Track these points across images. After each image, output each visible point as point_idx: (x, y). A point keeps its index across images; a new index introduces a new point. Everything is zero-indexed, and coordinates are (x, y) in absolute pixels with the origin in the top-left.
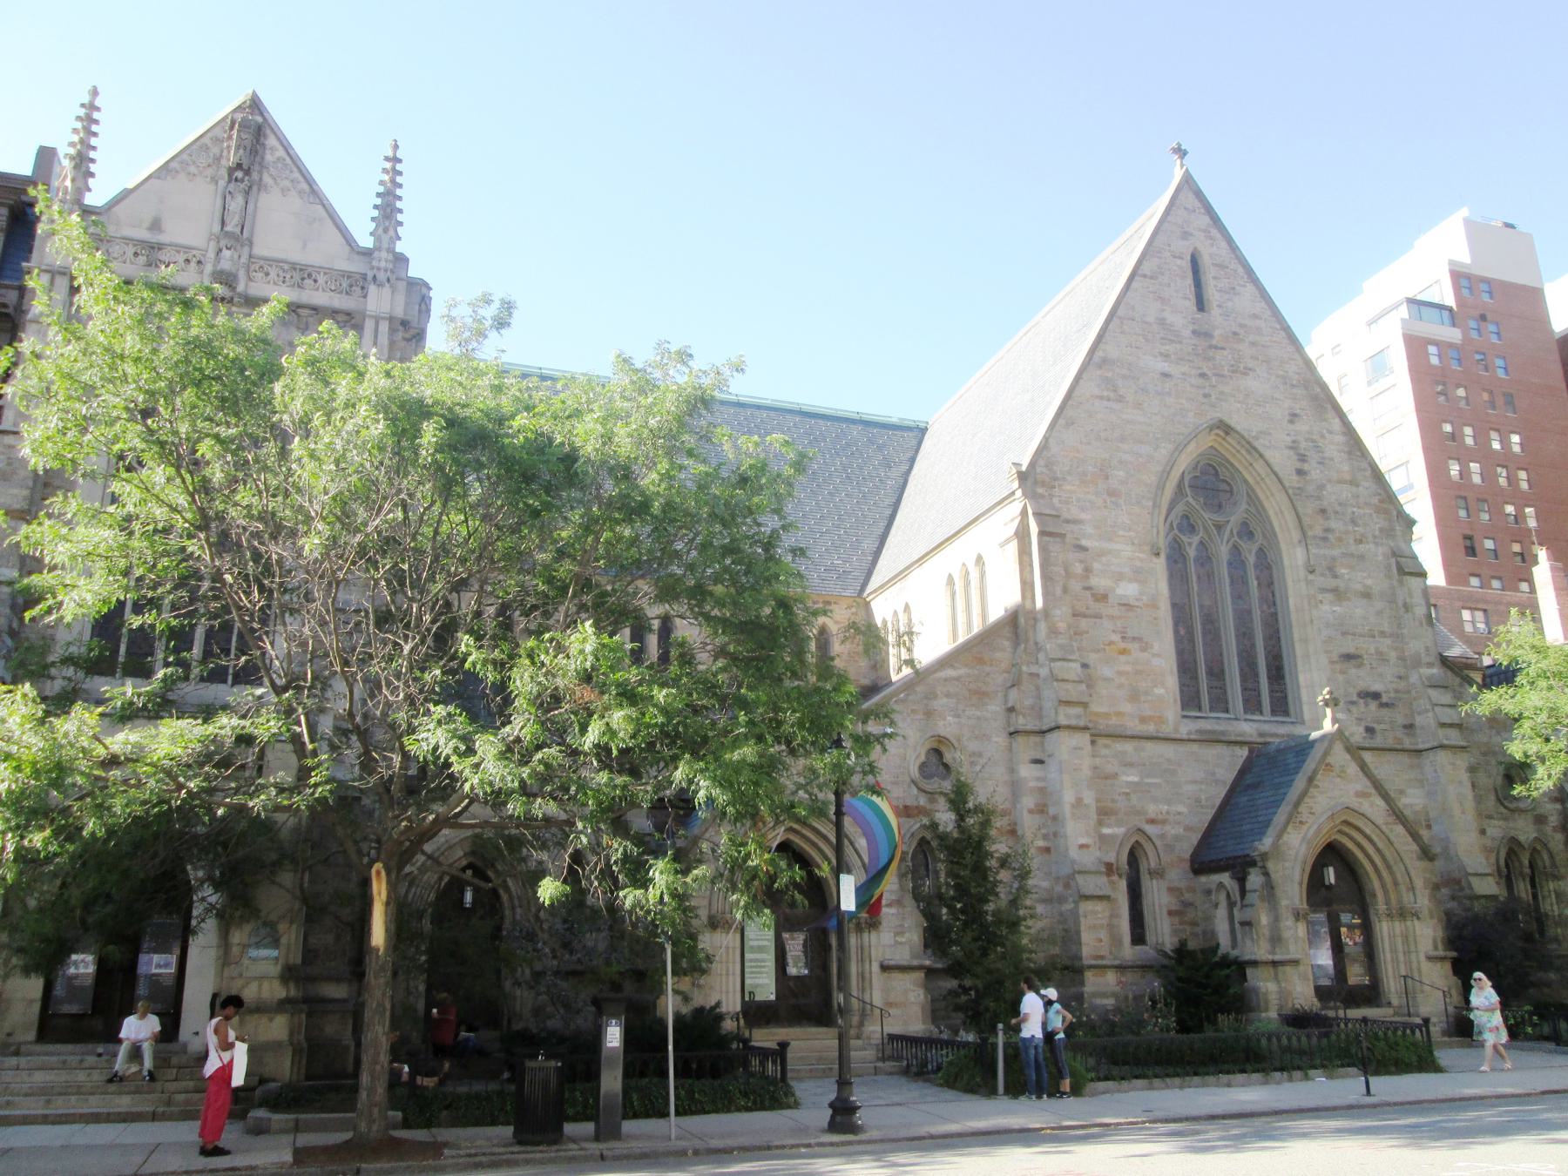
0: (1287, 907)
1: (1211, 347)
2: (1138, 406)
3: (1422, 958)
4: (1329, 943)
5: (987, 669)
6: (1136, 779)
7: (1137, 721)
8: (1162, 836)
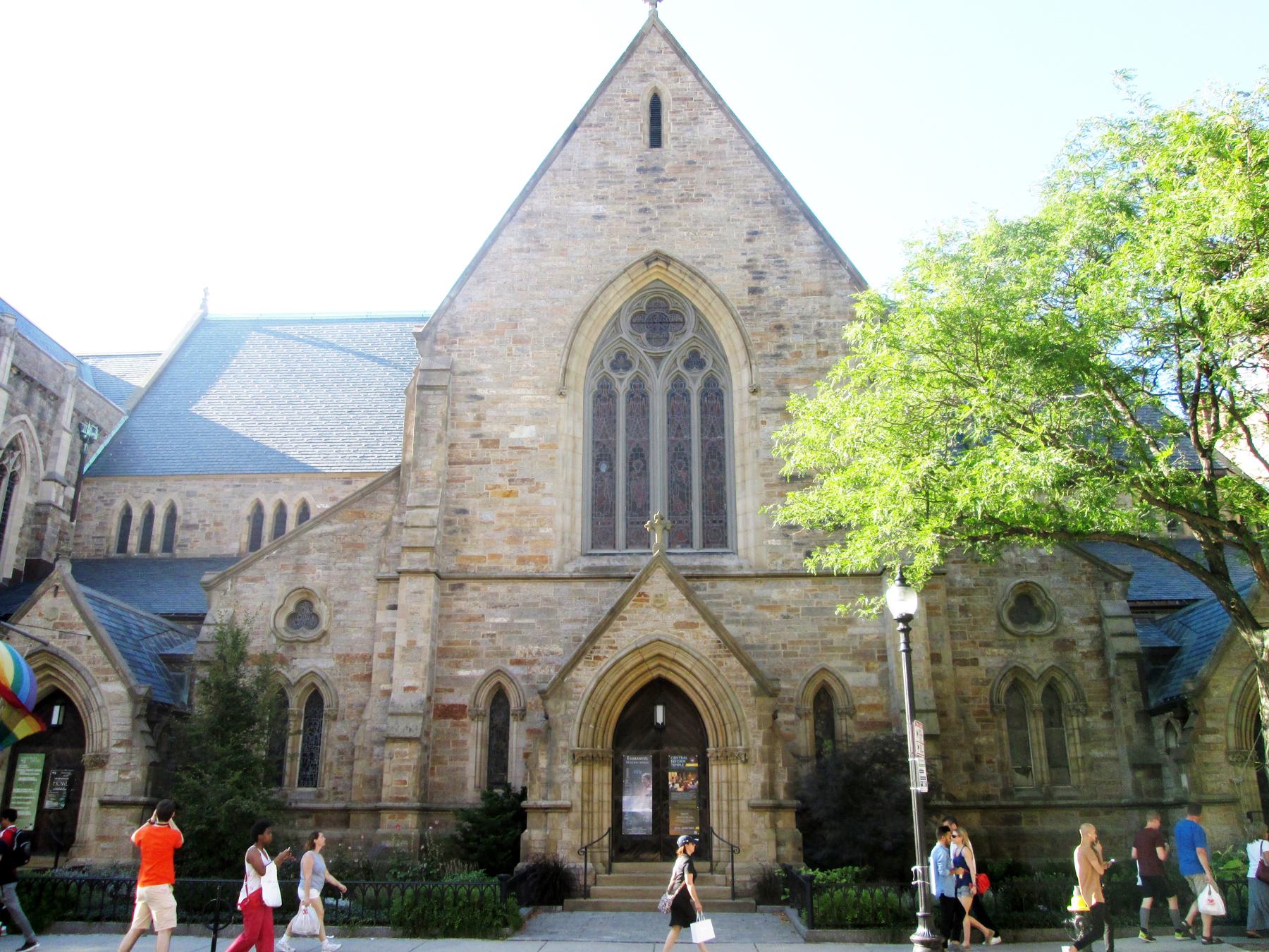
0: (565, 749)
2: (563, 252)
3: (744, 806)
4: (650, 789)
5: (366, 522)
6: (505, 620)
7: (515, 562)
8: (528, 678)
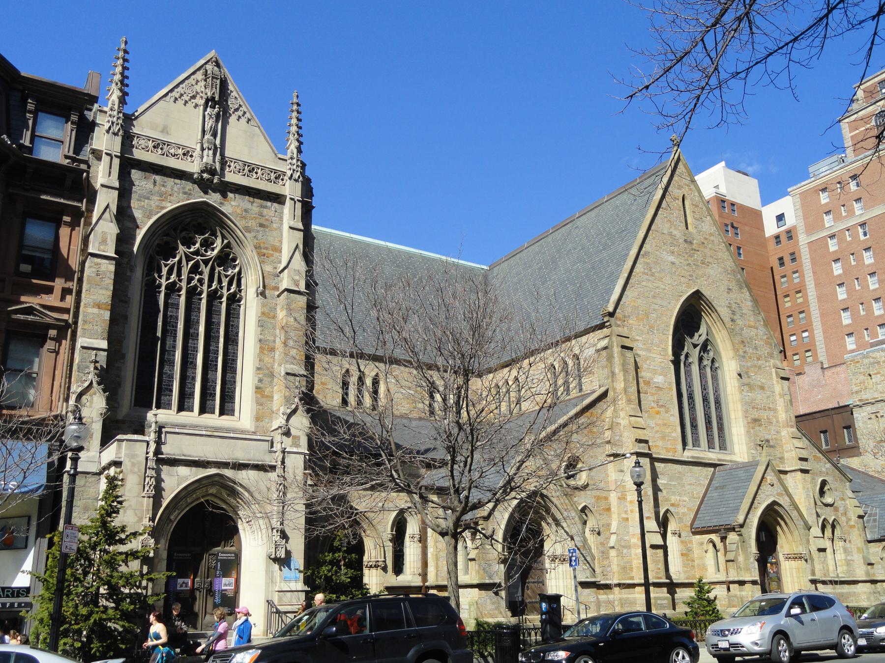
1: (692, 249)
6: (665, 482)
